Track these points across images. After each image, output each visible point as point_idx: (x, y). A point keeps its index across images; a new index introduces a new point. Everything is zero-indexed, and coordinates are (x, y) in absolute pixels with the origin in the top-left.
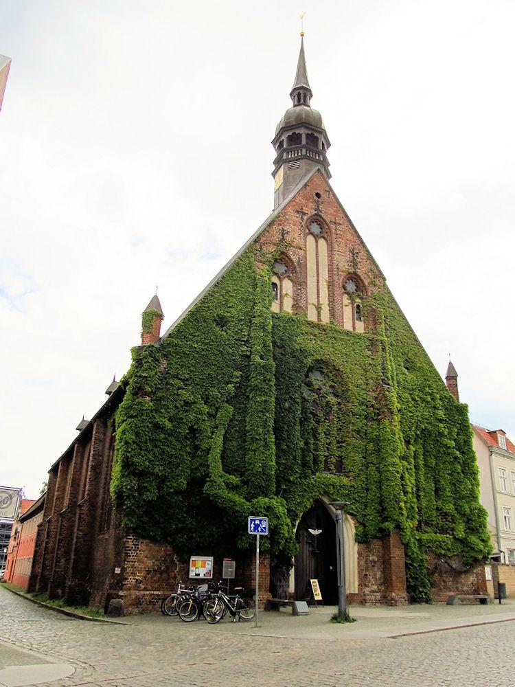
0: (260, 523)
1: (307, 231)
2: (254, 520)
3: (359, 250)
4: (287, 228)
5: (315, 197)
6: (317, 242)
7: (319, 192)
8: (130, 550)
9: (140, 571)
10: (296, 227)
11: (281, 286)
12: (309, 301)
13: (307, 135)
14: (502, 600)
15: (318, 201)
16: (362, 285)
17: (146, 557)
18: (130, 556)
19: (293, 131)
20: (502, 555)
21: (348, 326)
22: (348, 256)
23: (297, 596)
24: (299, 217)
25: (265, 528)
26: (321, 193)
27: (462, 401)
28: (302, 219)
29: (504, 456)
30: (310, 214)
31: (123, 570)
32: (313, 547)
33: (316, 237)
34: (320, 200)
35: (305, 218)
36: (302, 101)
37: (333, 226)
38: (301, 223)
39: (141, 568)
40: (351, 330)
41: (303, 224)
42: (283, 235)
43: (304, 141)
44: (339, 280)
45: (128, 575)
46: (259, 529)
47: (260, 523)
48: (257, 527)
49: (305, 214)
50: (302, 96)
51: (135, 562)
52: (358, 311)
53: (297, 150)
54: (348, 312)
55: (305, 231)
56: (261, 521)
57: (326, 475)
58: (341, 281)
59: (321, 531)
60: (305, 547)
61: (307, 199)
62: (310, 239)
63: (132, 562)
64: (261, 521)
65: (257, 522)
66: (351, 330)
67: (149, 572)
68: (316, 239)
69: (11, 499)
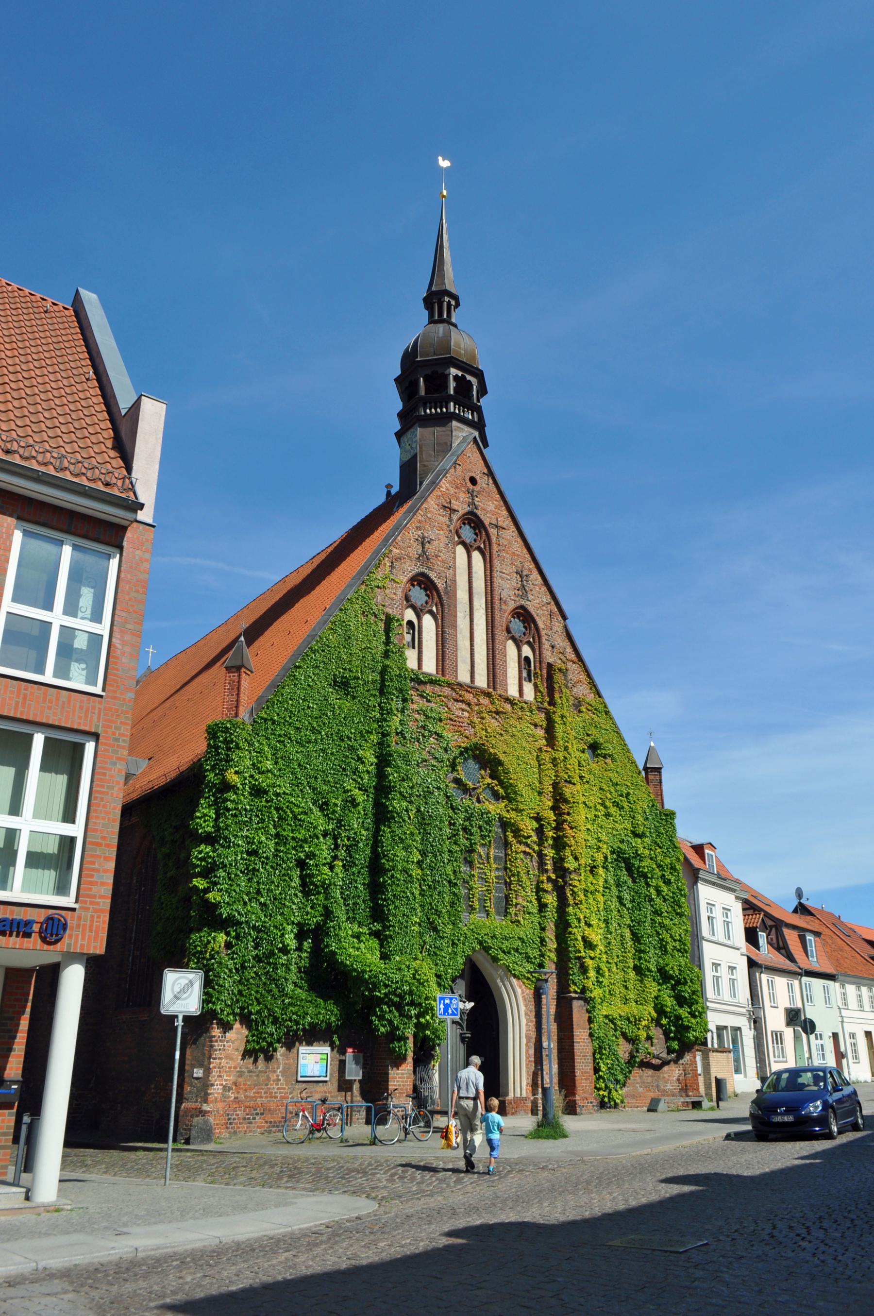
1: (456, 539)
2: (444, 999)
3: (530, 570)
4: (430, 534)
5: (469, 484)
7: (474, 475)
9: (228, 1073)
10: (441, 532)
11: (420, 627)
14: (720, 1103)
15: (473, 491)
20: (709, 1035)
21: (513, 691)
22: (515, 581)
26: (477, 478)
27: (668, 805)
28: (450, 519)
30: (461, 512)
31: (208, 1071)
32: (462, 1029)
33: (468, 549)
34: (476, 488)
35: (455, 517)
37: (493, 531)
39: (230, 1068)
40: (517, 694)
41: (452, 527)
42: (423, 544)
44: (503, 618)
45: (214, 1079)
46: (450, 1011)
47: (451, 1002)
48: (447, 1007)
56: (451, 999)
57: (478, 918)
58: (504, 619)
59: (472, 1004)
61: (457, 487)
62: (460, 550)
64: (451, 999)
65: (447, 1001)
69: (192, 985)
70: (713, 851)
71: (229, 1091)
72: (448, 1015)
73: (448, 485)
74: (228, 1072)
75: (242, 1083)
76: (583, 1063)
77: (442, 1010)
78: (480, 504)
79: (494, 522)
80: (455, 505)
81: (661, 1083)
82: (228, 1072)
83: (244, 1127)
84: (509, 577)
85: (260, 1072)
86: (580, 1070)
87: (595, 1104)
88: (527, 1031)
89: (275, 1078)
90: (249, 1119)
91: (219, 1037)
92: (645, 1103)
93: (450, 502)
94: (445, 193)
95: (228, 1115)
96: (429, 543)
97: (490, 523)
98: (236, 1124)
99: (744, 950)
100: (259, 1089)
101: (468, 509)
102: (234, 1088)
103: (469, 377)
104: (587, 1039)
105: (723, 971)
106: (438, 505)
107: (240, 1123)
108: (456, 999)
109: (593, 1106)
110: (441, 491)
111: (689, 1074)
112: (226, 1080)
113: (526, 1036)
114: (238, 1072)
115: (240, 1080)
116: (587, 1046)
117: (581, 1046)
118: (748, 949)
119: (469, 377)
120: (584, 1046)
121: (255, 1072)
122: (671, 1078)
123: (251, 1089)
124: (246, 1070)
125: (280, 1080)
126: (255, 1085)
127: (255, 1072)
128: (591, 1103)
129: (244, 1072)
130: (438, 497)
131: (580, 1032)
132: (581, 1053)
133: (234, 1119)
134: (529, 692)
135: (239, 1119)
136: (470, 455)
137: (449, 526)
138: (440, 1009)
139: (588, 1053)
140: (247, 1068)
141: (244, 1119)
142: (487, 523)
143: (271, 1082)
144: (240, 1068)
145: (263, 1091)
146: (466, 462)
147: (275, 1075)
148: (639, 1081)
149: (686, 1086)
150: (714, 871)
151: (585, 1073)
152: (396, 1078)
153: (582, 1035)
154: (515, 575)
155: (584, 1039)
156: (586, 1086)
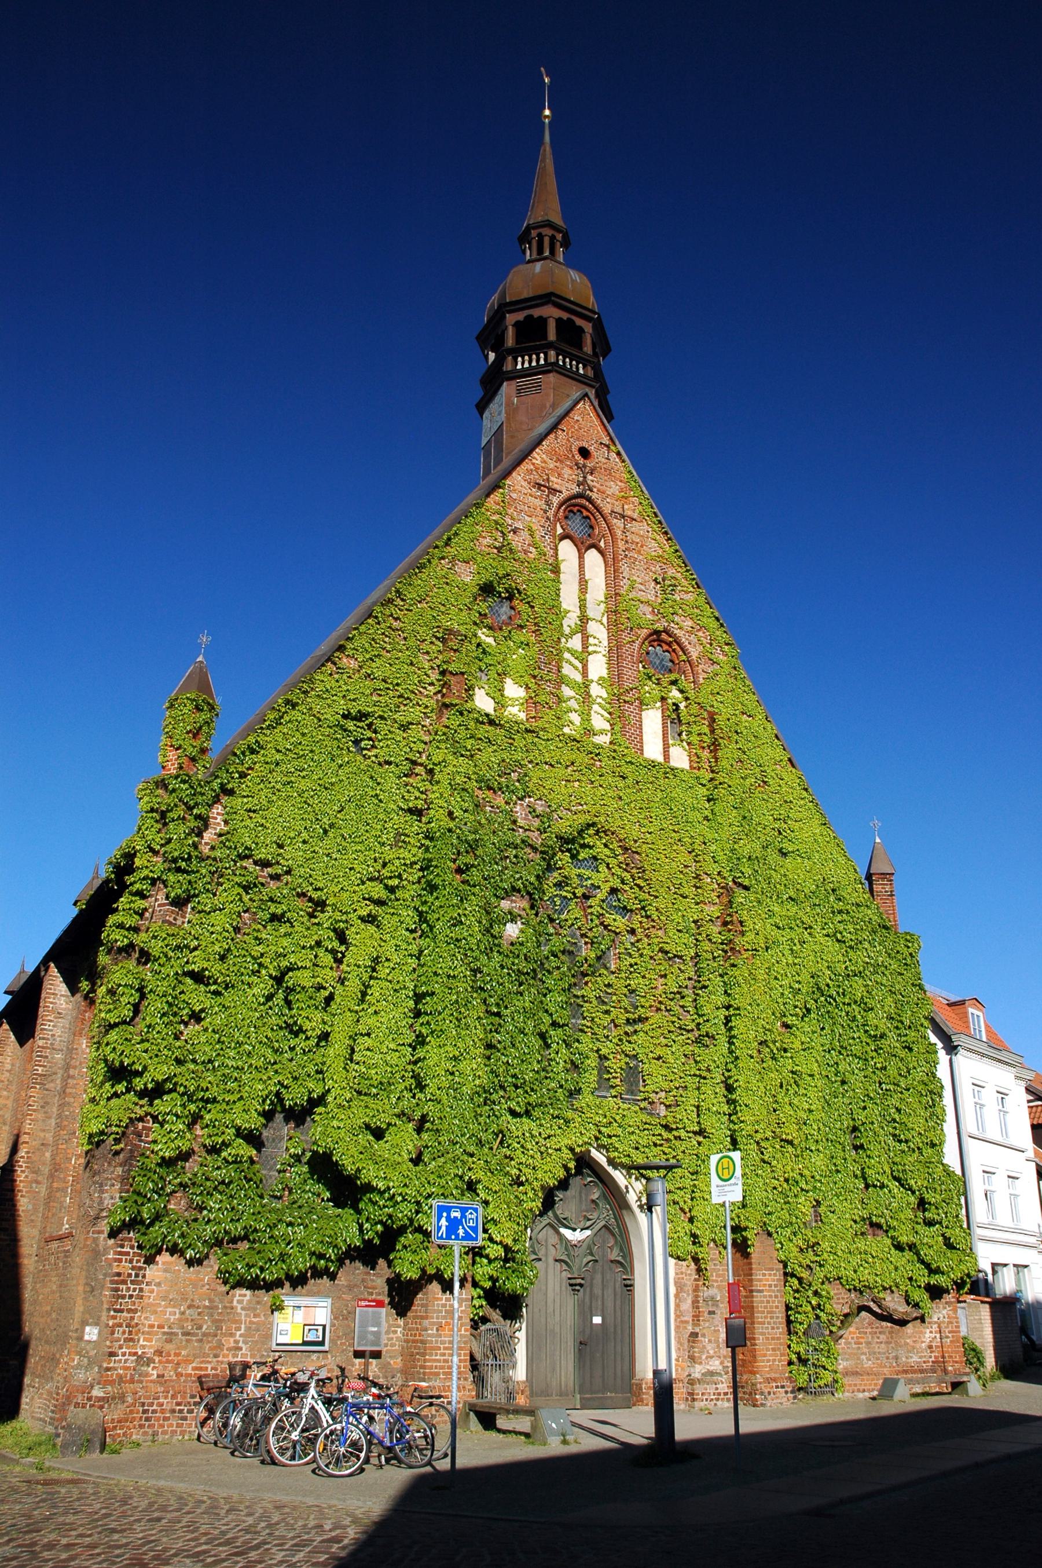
0: (463, 1216)
2: (448, 1209)
5: (578, 457)
6: (581, 557)
7: (585, 445)
8: (124, 1282)
12: (605, 660)
13: (559, 321)
15: (585, 466)
16: (684, 658)
17: (164, 1298)
18: (123, 1297)
19: (527, 313)
23: (531, 1387)
24: (541, 497)
25: (475, 1229)
26: (592, 449)
28: (548, 503)
29: (983, 1055)
30: (565, 494)
34: (590, 464)
35: (556, 500)
36: (547, 253)
37: (618, 524)
38: (545, 511)
40: (660, 759)
41: (551, 514)
43: (552, 336)
46: (461, 1232)
47: (463, 1216)
49: (554, 491)
50: (546, 240)
51: (135, 1311)
52: (673, 718)
53: (536, 350)
54: (652, 721)
55: (555, 529)
56: (464, 1211)
60: (551, 1271)
63: (129, 1311)
64: (464, 1211)
66: (660, 759)
67: (170, 1337)
68: (579, 550)
70: (981, 1010)
71: (148, 1365)
72: (457, 1238)
73: (544, 456)
74: (148, 1333)
75: (172, 1353)
76: (769, 1323)
77: (444, 1229)
78: (595, 484)
79: (619, 510)
80: (555, 482)
81: (901, 1352)
82: (148, 1333)
83: (171, 1425)
84: (643, 588)
85: (204, 1334)
86: (763, 1334)
87: (789, 1390)
88: (677, 1274)
89: (232, 1345)
90: (181, 1411)
91: (130, 1275)
92: (876, 1384)
93: (548, 480)
94: (878, 840)
95: (143, 1404)
96: (515, 533)
97: (612, 512)
98: (158, 1420)
99: (1030, 1154)
100: (202, 1362)
101: (576, 490)
102: (157, 1359)
103: (579, 322)
104: (776, 1286)
105: (999, 1182)
106: (529, 483)
107: (166, 1419)
108: (476, 1210)
109: (786, 1392)
110: (533, 464)
111: (947, 1337)
112: (144, 1347)
113: (676, 1283)
114: (164, 1333)
115: (169, 1347)
116: (776, 1297)
117: (765, 1296)
118: (1036, 1153)
119: (579, 322)
120: (770, 1296)
121: (197, 1335)
122: (918, 1346)
123: (188, 1362)
124: (179, 1331)
125: (241, 1349)
126: (195, 1356)
127: (197, 1335)
128: (783, 1387)
129: (176, 1334)
130: (530, 472)
131: (764, 1275)
132: (765, 1307)
133: (154, 1412)
134: (680, 758)
135: (163, 1411)
136: (579, 418)
137: (545, 511)
138: (439, 1228)
139: (777, 1307)
140: (183, 1327)
141: (173, 1411)
142: (607, 509)
143: (225, 1352)
144: (170, 1327)
145: (209, 1366)
146: (572, 427)
147: (232, 1340)
148: (865, 1350)
149: (943, 1357)
150: (981, 1036)
151: (773, 1339)
152: (439, 1348)
153: (767, 1280)
154: (653, 584)
155: (770, 1286)
156: (774, 1360)
